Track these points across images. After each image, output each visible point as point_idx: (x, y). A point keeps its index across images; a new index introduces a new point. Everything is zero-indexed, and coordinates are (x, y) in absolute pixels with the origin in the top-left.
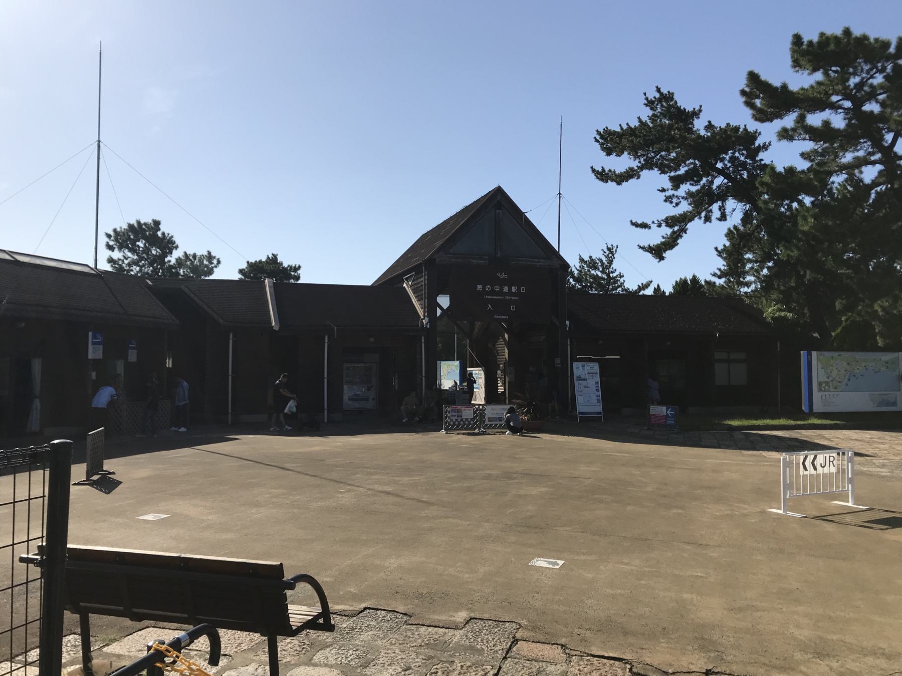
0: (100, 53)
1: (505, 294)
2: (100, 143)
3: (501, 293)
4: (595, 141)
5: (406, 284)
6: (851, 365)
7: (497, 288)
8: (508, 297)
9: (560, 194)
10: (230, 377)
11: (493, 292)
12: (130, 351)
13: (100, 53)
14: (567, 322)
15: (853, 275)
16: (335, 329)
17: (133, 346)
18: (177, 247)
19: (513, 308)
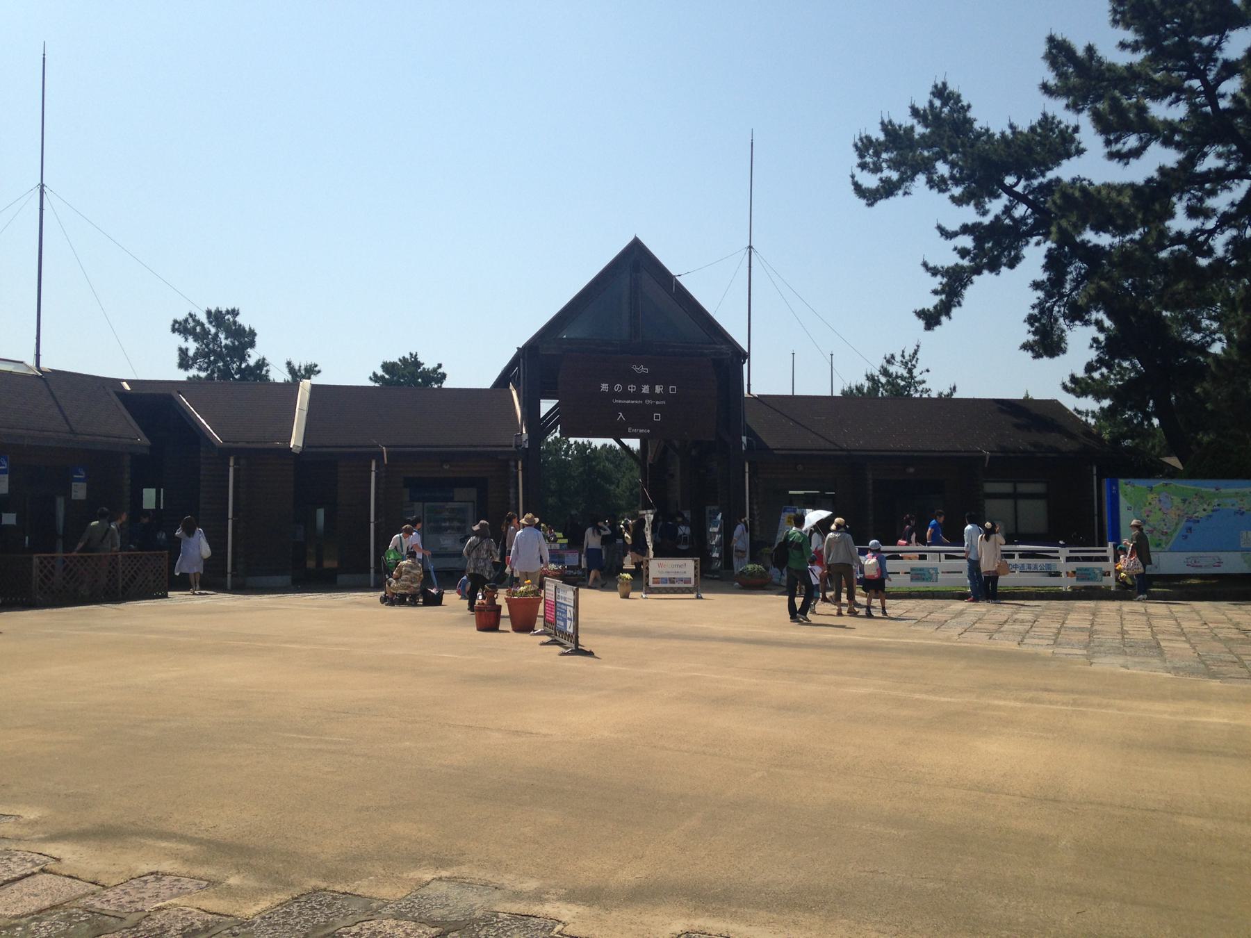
0: (44, 58)
1: (645, 397)
2: (45, 188)
3: (638, 395)
6: (1190, 503)
7: (632, 388)
8: (648, 402)
9: (750, 247)
10: (230, 522)
11: (625, 395)
12: (73, 484)
13: (44, 58)
14: (744, 439)
15: (210, 336)
16: (385, 451)
17: (80, 477)
19: (657, 417)
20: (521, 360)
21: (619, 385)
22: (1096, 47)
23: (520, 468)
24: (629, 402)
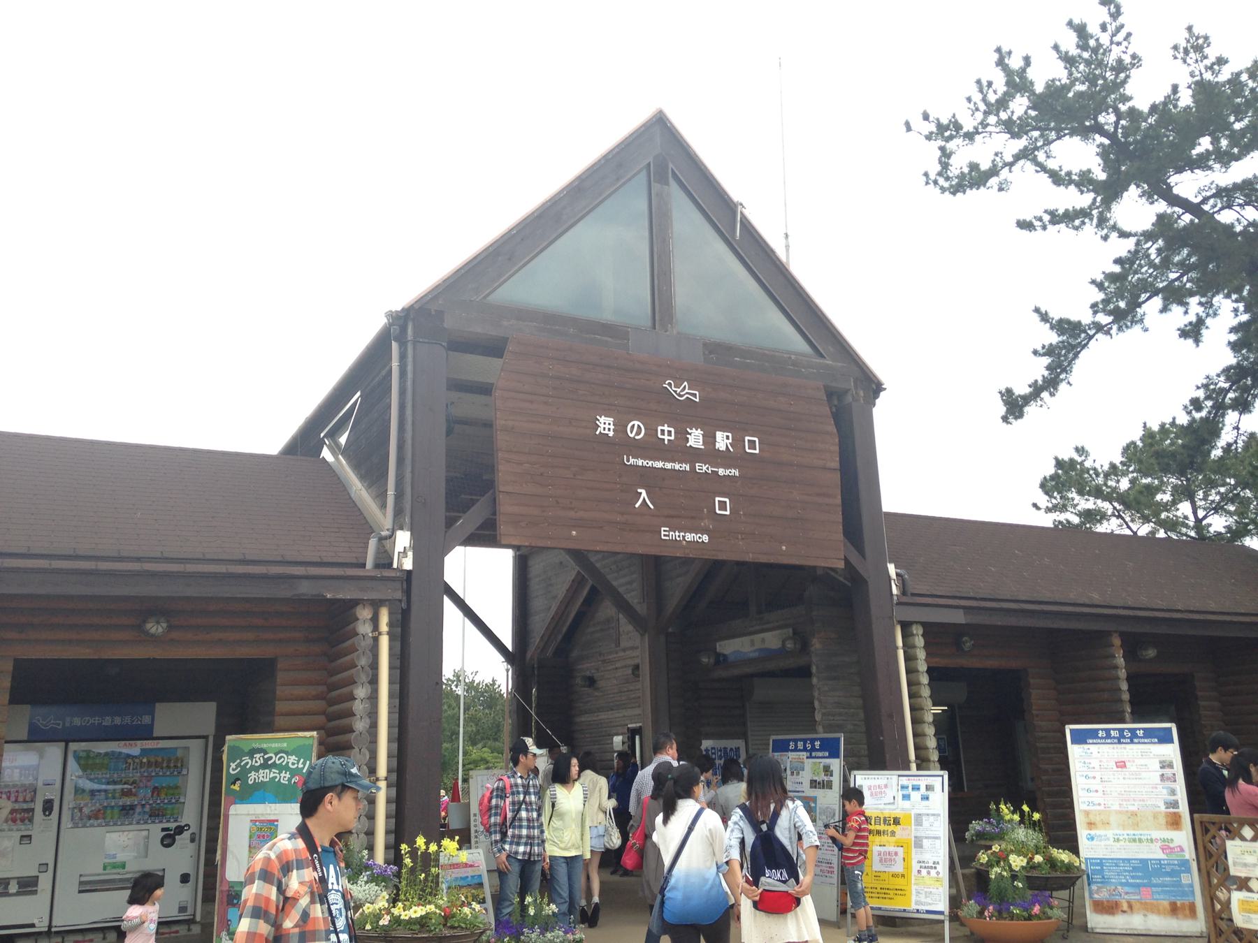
1: (693, 455)
3: (679, 450)
4: (1119, 237)
5: (330, 448)
7: (666, 433)
8: (702, 468)
11: (652, 447)
14: (892, 569)
18: (1089, 171)
20: (395, 345)
21: (636, 423)
22: (1021, 218)
23: (384, 627)
24: (659, 464)
